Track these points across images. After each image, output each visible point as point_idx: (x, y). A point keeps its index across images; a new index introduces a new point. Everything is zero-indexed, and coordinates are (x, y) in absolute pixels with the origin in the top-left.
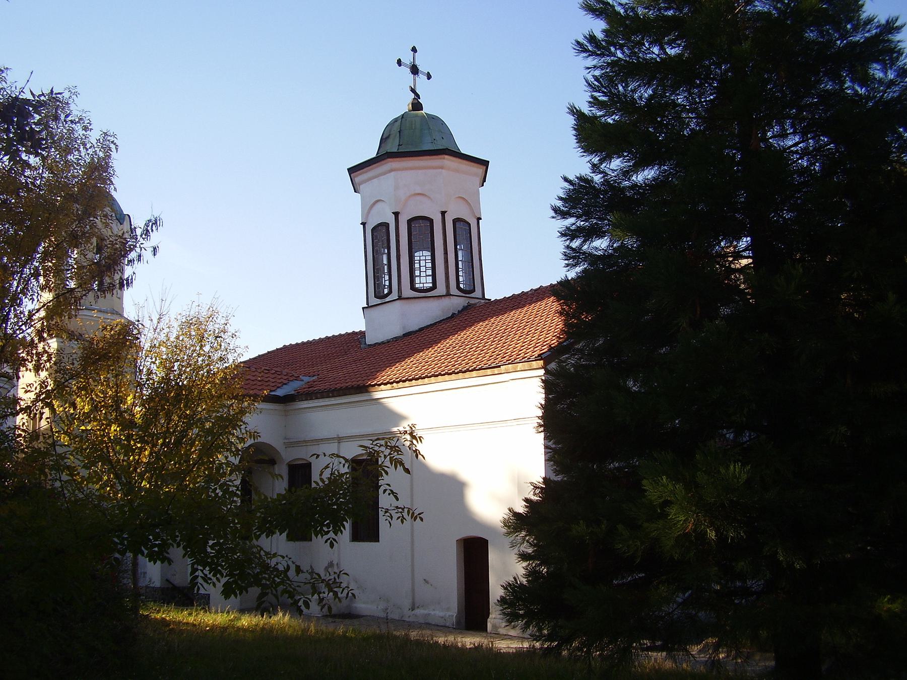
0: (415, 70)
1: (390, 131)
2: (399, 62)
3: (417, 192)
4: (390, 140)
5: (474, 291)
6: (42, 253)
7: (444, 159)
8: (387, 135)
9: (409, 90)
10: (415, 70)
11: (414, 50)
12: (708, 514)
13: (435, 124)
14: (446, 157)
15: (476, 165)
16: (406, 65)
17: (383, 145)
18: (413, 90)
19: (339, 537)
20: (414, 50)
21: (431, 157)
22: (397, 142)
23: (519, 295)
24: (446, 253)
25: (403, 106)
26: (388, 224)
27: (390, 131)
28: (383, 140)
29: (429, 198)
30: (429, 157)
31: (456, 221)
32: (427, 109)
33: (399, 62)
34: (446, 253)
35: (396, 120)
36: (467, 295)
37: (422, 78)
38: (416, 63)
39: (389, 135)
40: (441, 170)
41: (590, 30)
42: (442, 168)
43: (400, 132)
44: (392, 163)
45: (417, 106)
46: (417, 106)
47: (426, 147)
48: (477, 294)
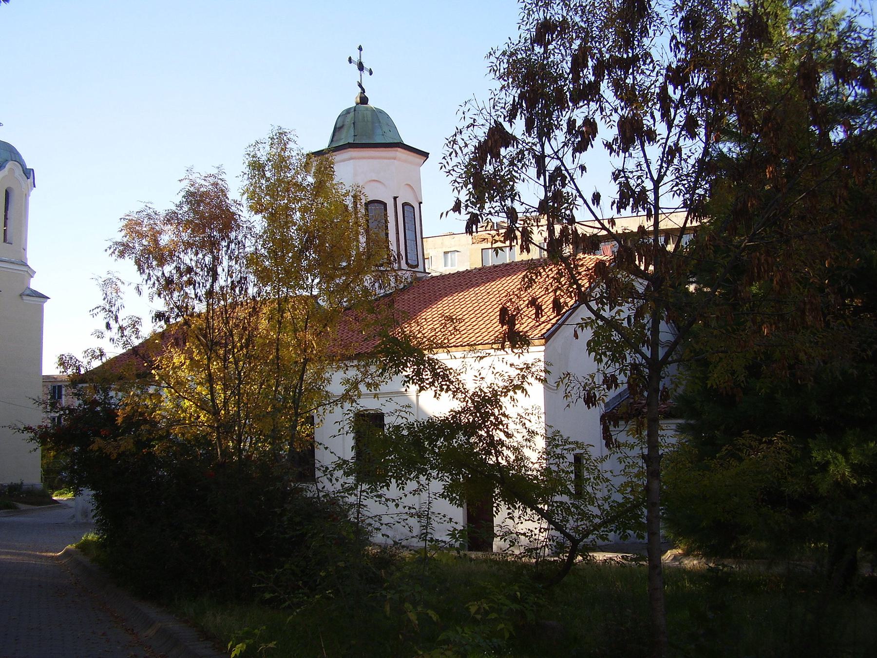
0: (361, 67)
1: (343, 122)
2: (350, 60)
3: (373, 179)
4: (344, 132)
5: (417, 266)
6: (512, 206)
7: (397, 151)
8: (341, 125)
9: (357, 84)
10: (361, 67)
11: (360, 49)
12: (650, 11)
13: (379, 116)
14: (399, 149)
15: (415, 155)
16: (355, 62)
17: (337, 134)
18: (360, 85)
19: (395, 377)
20: (360, 49)
21: (387, 149)
22: (352, 133)
23: (463, 272)
24: (398, 233)
25: (351, 101)
26: (402, 204)
27: (343, 122)
28: (337, 129)
29: (384, 185)
30: (384, 149)
31: (405, 205)
32: (372, 103)
33: (350, 60)
34: (398, 233)
35: (348, 111)
36: (412, 269)
37: (366, 73)
38: (362, 60)
39: (343, 125)
40: (393, 160)
41: (649, 221)
42: (395, 159)
43: (354, 123)
44: (352, 153)
45: (364, 100)
46: (364, 100)
47: (379, 140)
48: (421, 268)
